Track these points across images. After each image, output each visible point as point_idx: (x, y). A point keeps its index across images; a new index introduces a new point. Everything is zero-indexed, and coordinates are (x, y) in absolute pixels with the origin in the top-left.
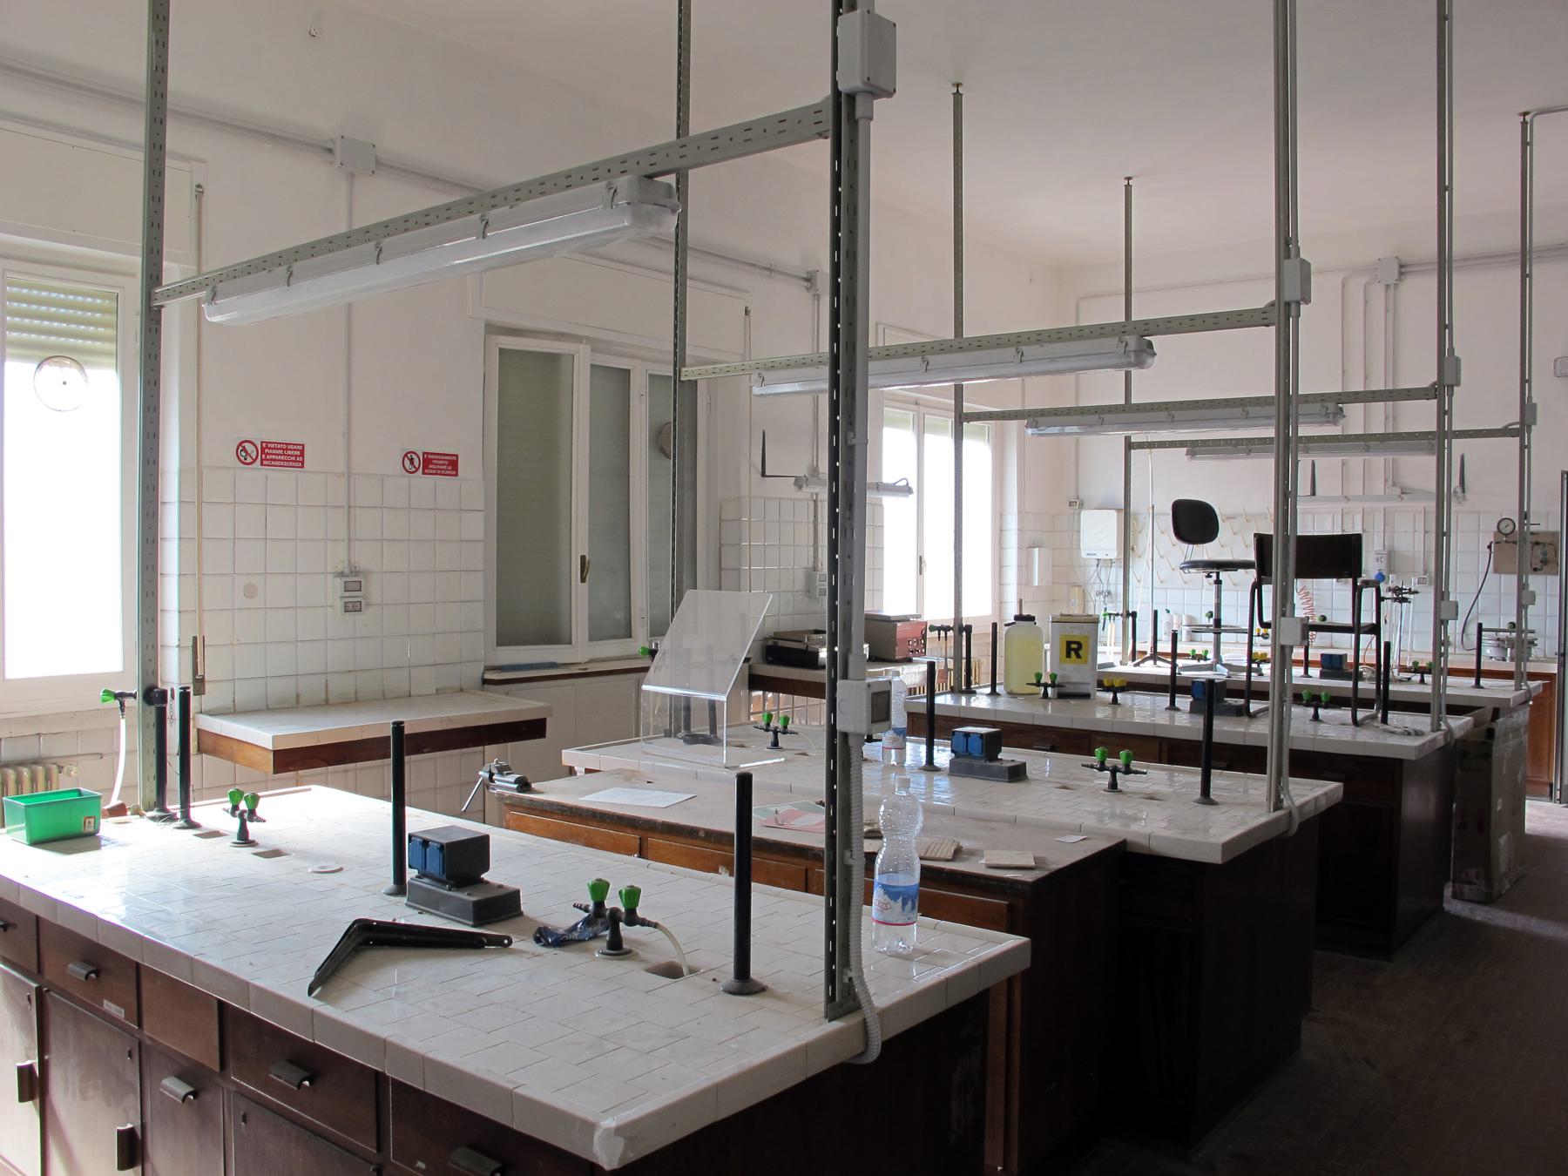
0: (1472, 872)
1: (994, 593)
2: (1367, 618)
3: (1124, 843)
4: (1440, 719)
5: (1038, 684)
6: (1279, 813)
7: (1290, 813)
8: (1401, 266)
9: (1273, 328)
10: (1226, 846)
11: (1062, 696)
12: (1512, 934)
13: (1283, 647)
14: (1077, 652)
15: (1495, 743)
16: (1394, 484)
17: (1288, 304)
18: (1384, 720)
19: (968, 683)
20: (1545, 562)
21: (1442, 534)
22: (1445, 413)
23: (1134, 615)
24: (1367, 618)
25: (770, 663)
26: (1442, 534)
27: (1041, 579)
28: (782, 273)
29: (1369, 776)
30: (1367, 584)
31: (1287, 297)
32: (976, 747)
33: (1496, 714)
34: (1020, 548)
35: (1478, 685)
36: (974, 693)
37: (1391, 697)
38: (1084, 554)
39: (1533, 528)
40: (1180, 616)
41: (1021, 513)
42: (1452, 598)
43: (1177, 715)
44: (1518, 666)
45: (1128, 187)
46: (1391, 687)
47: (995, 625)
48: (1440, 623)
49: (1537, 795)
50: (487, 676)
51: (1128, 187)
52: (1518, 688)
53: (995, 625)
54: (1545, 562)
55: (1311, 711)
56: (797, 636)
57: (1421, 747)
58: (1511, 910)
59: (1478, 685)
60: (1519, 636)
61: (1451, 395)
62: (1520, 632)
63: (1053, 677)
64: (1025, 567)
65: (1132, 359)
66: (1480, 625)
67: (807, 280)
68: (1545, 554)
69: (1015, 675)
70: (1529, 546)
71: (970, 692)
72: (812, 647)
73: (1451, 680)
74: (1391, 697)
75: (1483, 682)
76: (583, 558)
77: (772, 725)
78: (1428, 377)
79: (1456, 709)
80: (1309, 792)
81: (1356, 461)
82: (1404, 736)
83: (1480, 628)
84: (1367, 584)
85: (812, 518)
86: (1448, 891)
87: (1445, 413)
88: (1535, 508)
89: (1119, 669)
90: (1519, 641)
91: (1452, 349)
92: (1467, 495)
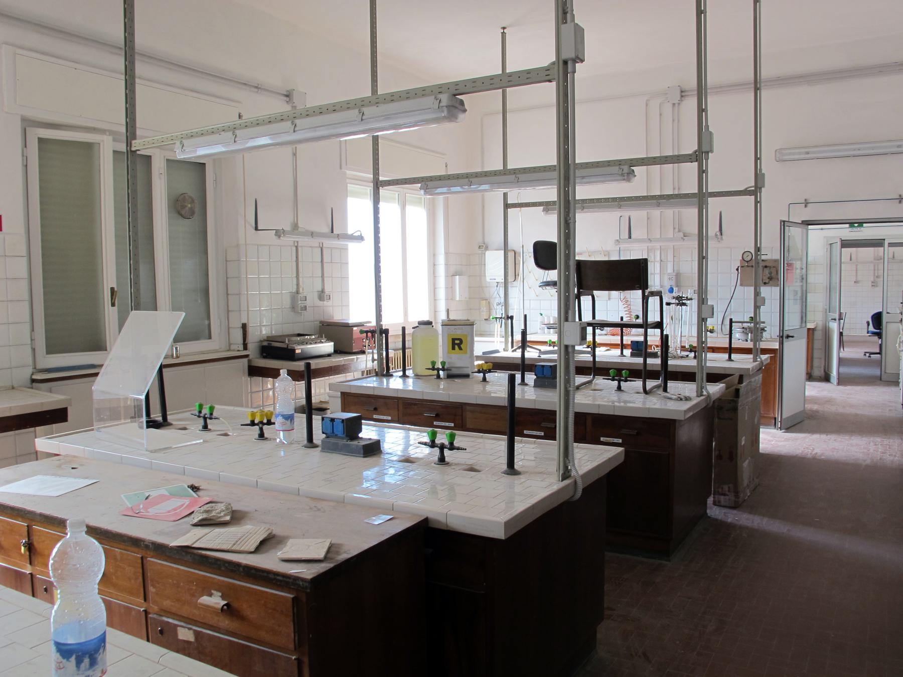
0: (726, 488)
1: (430, 304)
2: (653, 317)
3: (426, 520)
4: (702, 388)
5: (433, 369)
6: (567, 482)
7: (575, 482)
8: (682, 92)
9: (554, 84)
10: (507, 524)
11: (450, 376)
12: (752, 532)
13: (567, 347)
14: (459, 345)
15: (740, 399)
16: (679, 231)
17: (565, 63)
18: (665, 390)
19: (388, 368)
20: (770, 278)
21: (702, 258)
22: (703, 172)
23: (512, 318)
24: (653, 317)
25: (265, 357)
26: (702, 258)
27: (461, 295)
28: (265, 90)
29: (643, 436)
30: (653, 294)
31: (564, 56)
32: (339, 429)
33: (741, 379)
34: (446, 276)
35: (730, 359)
36: (392, 375)
37: (670, 369)
38: (488, 279)
39: (763, 257)
40: (549, 317)
41: (447, 253)
42: (709, 303)
43: (526, 388)
44: (755, 345)
45: (503, 34)
46: (670, 362)
47: (404, 329)
48: (702, 320)
49: (767, 425)
50: (34, 377)
51: (503, 34)
52: (755, 360)
53: (404, 329)
54: (770, 278)
55: (616, 383)
56: (280, 338)
57: (689, 410)
58: (751, 513)
59: (730, 359)
60: (755, 326)
61: (707, 159)
62: (756, 323)
63: (443, 363)
64: (450, 288)
65: (445, 114)
66: (731, 320)
67: (287, 96)
68: (770, 273)
69: (419, 362)
70: (761, 269)
71: (389, 375)
72: (291, 346)
73: (710, 355)
74: (670, 369)
75: (733, 356)
76: (112, 289)
77: (204, 412)
78: (690, 147)
79: (714, 377)
80: (591, 458)
81: (656, 213)
82: (678, 401)
83: (731, 321)
84: (653, 294)
85: (295, 259)
86: (710, 500)
87: (703, 172)
88: (765, 245)
89: (503, 354)
90: (756, 329)
91: (707, 126)
92: (724, 237)
